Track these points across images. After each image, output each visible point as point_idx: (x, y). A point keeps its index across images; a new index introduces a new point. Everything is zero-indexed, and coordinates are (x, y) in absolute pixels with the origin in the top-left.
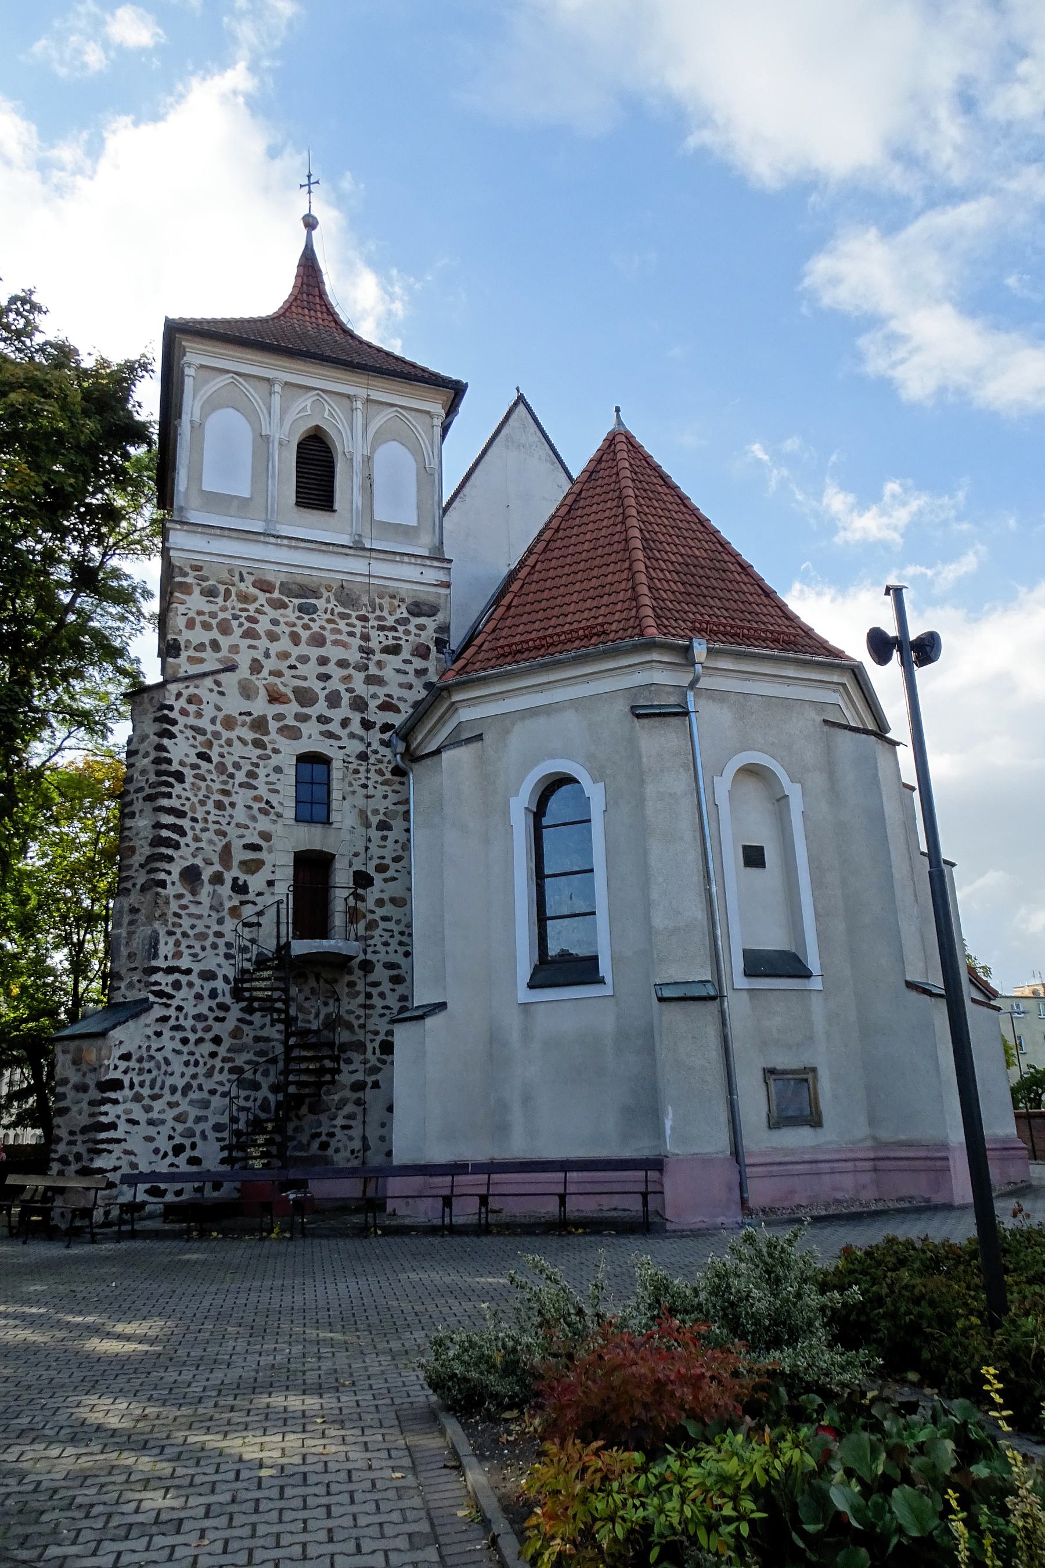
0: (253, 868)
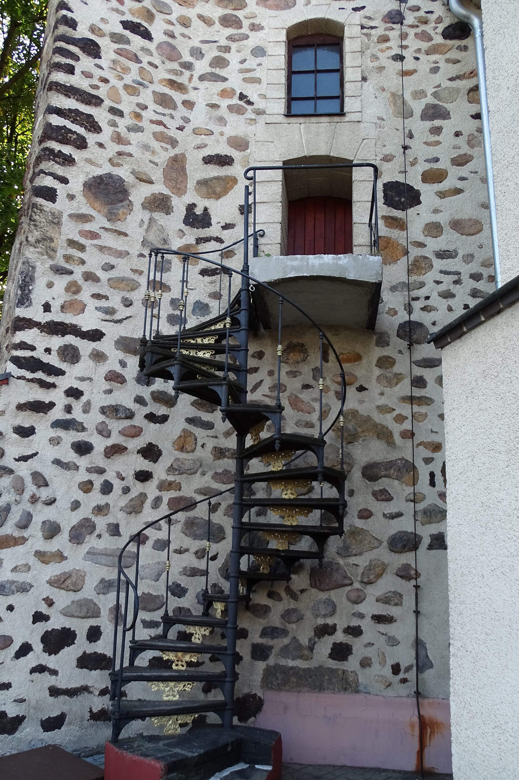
0: (218, 189)
